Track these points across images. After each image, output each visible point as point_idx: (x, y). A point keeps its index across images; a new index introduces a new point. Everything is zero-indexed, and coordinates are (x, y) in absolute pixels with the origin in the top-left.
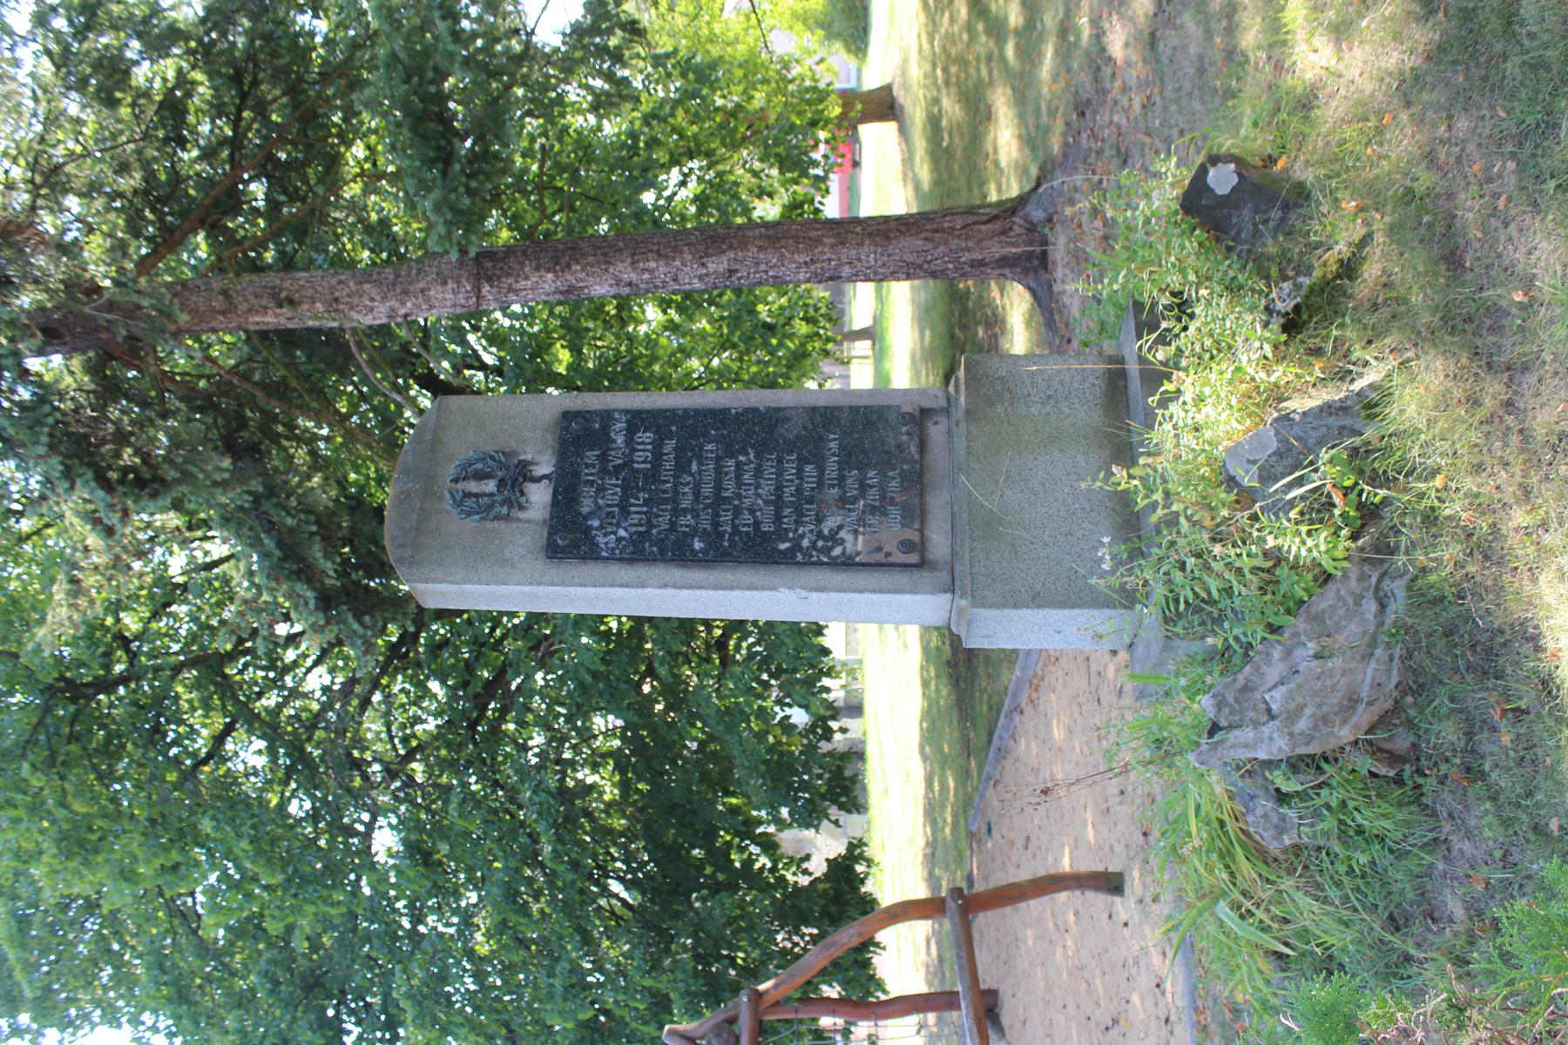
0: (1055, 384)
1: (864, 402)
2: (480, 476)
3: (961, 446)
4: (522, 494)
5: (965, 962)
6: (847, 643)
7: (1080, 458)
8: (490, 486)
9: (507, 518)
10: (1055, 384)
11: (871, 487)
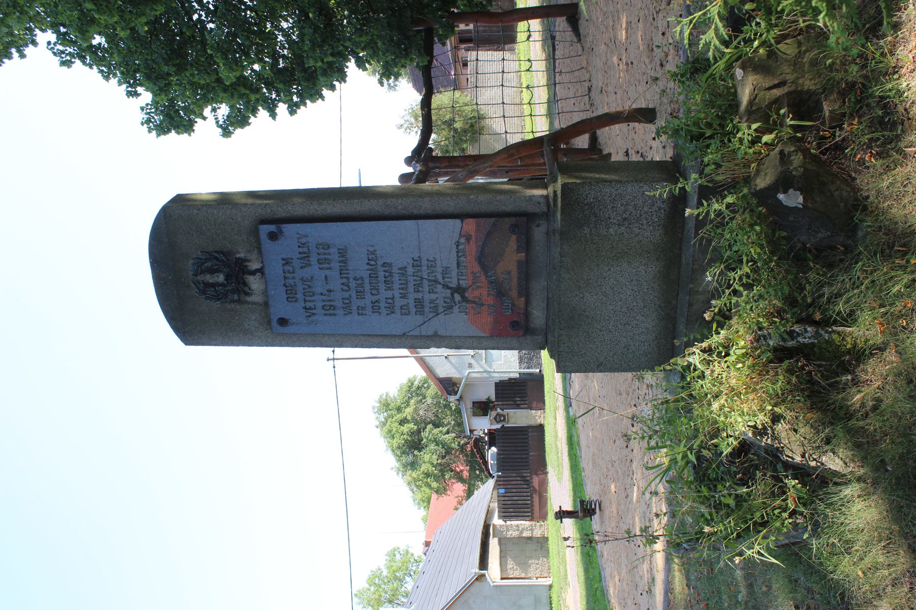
2: (212, 271)
4: (245, 284)
8: (221, 278)
9: (239, 301)
10: (630, 208)
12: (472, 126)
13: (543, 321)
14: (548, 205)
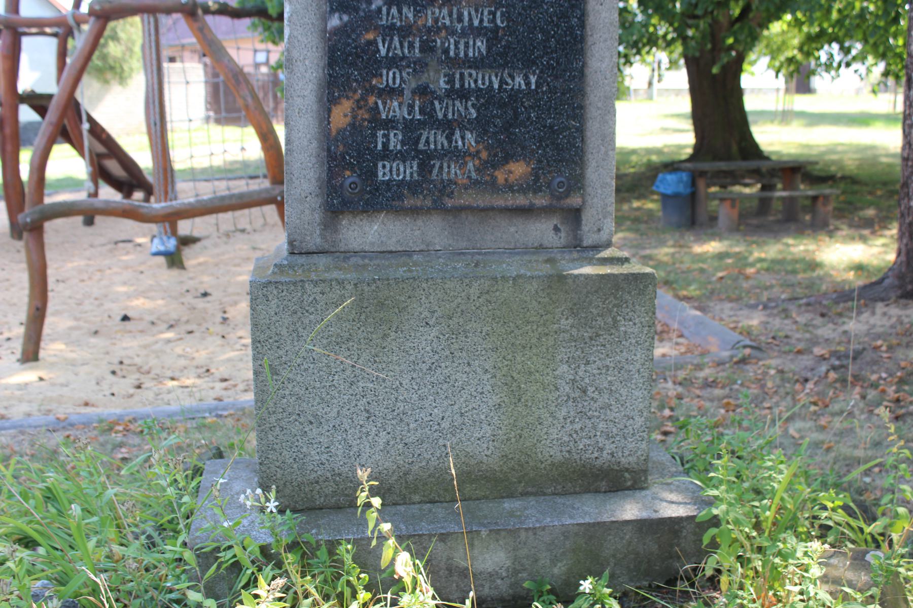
0: (605, 398)
1: (593, 127)
3: (513, 267)
5: (227, 202)
6: (667, 90)
7: (487, 430)
10: (605, 398)
11: (449, 138)
12: (112, 68)
13: (355, 245)
14: (597, 247)
